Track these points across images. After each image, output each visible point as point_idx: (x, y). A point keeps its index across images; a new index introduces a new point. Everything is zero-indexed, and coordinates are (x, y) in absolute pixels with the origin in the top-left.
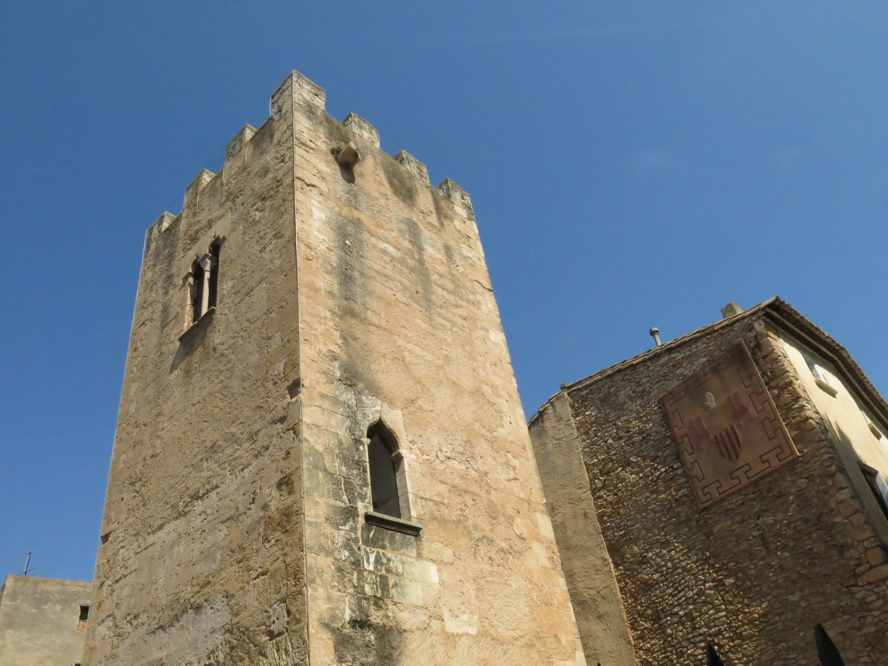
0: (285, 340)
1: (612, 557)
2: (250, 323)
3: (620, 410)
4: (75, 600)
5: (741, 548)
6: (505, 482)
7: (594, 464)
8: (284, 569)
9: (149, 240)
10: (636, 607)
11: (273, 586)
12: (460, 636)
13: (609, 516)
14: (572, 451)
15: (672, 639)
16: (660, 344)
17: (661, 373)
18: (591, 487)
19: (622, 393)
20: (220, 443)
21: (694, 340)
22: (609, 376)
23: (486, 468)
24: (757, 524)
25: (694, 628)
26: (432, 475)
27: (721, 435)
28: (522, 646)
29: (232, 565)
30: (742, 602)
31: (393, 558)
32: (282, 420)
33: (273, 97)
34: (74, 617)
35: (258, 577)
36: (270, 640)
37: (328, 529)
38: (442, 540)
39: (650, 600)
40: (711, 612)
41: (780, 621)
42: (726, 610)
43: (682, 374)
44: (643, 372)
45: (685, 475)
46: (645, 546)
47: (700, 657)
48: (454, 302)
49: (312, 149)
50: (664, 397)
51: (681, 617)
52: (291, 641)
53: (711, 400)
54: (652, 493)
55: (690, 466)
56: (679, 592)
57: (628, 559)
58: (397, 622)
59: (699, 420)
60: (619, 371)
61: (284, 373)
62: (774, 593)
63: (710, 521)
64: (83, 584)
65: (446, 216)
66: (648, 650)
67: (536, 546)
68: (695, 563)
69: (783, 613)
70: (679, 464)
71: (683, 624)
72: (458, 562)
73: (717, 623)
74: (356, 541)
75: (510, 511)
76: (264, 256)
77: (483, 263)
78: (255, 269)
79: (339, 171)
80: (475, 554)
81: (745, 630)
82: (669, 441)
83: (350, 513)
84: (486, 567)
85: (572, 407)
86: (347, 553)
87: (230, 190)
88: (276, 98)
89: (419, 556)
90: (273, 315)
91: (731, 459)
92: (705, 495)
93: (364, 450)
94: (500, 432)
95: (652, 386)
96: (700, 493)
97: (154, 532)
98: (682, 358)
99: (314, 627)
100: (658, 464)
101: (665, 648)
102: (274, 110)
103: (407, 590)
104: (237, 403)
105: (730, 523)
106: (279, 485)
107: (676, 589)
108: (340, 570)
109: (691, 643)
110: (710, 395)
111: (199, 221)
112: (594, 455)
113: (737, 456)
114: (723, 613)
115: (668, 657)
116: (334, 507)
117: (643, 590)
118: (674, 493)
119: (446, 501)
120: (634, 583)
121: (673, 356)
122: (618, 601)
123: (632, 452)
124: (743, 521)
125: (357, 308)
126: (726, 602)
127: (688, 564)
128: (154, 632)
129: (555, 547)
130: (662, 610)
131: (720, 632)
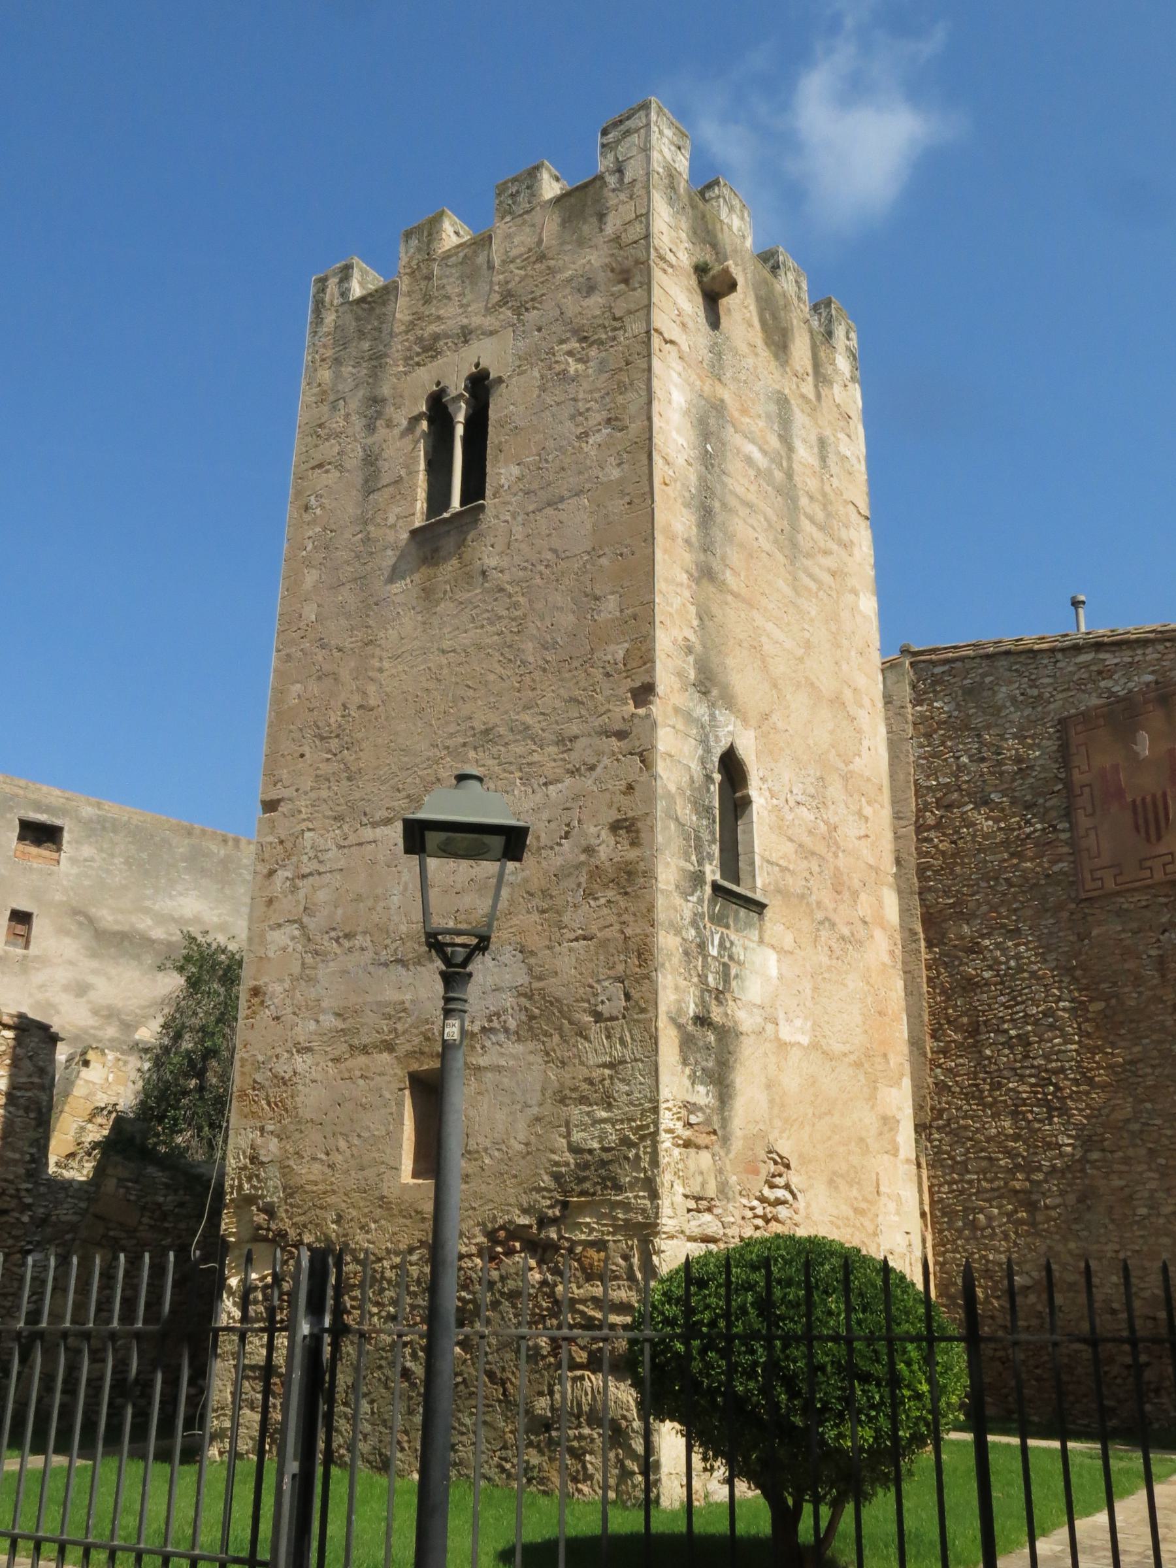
0: (629, 612)
1: (925, 931)
2: (558, 557)
3: (993, 715)
4: (11, 808)
5: (1127, 966)
6: (856, 841)
7: (929, 788)
8: (621, 941)
9: (319, 306)
10: (946, 1009)
11: (602, 958)
12: (792, 1045)
13: (936, 872)
14: (898, 757)
15: (990, 1063)
16: (1083, 629)
17: (1075, 678)
18: (917, 821)
19: (1004, 689)
20: (502, 730)
21: (1144, 643)
22: (988, 656)
23: (836, 819)
24: (1159, 941)
25: (1026, 1057)
26: (780, 828)
27: (1143, 799)
28: (850, 1065)
29: (528, 912)
30: (1104, 1039)
31: (736, 942)
32: (621, 735)
33: (605, 132)
34: (9, 834)
35: (577, 939)
36: (596, 1022)
37: (678, 900)
38: (784, 920)
39: (970, 1004)
40: (1057, 1041)
41: (1153, 1074)
42: (1079, 1043)
43: (1108, 689)
44: (1046, 666)
45: (1071, 842)
46: (981, 929)
47: (1024, 1096)
48: (822, 544)
49: (672, 266)
50: (1070, 717)
51: (1011, 1038)
52: (630, 1031)
53: (1144, 746)
54: (1013, 855)
55: (1082, 832)
56: (1018, 1004)
57: (951, 940)
58: (735, 1022)
59: (1116, 768)
60: (1008, 653)
61: (625, 665)
62: (1154, 1037)
63: (1090, 918)
64: (22, 783)
65: (824, 377)
66: (950, 1070)
67: (878, 934)
68: (1052, 970)
69: (1159, 1065)
70: (1067, 825)
71: (1011, 1048)
72: (797, 951)
73: (1061, 1056)
74: (702, 916)
75: (856, 884)
76: (586, 450)
77: (862, 467)
78: (566, 466)
79: (702, 308)
80: (815, 941)
81: (1100, 1075)
82: (1060, 786)
83: (697, 879)
84: (825, 960)
85: (914, 687)
86: (693, 932)
87: (510, 286)
88: (611, 137)
89: (761, 941)
90: (604, 561)
91: (1148, 840)
92: (1094, 880)
93: (714, 789)
94: (858, 764)
95: (1055, 693)
96: (1088, 876)
97: (374, 825)
98: (1116, 665)
99: (663, 1022)
100: (1034, 816)
101: (975, 1073)
102: (606, 163)
103: (747, 983)
104: (533, 681)
105: (1119, 928)
106: (615, 827)
107: (1014, 998)
108: (686, 953)
109: (1016, 1075)
110: (1144, 736)
111: (439, 318)
112: (932, 773)
113: (1159, 838)
114: (1074, 1047)
115: (977, 1085)
116: (684, 870)
117: (964, 988)
118: (1046, 865)
119: (791, 867)
120: (951, 976)
121: (1102, 656)
122: (921, 995)
123: (996, 786)
124: (1140, 931)
125: (716, 566)
126: (1081, 1032)
127: (1040, 969)
128: (386, 965)
129: (898, 936)
130: (985, 1022)
131: (1062, 1070)
